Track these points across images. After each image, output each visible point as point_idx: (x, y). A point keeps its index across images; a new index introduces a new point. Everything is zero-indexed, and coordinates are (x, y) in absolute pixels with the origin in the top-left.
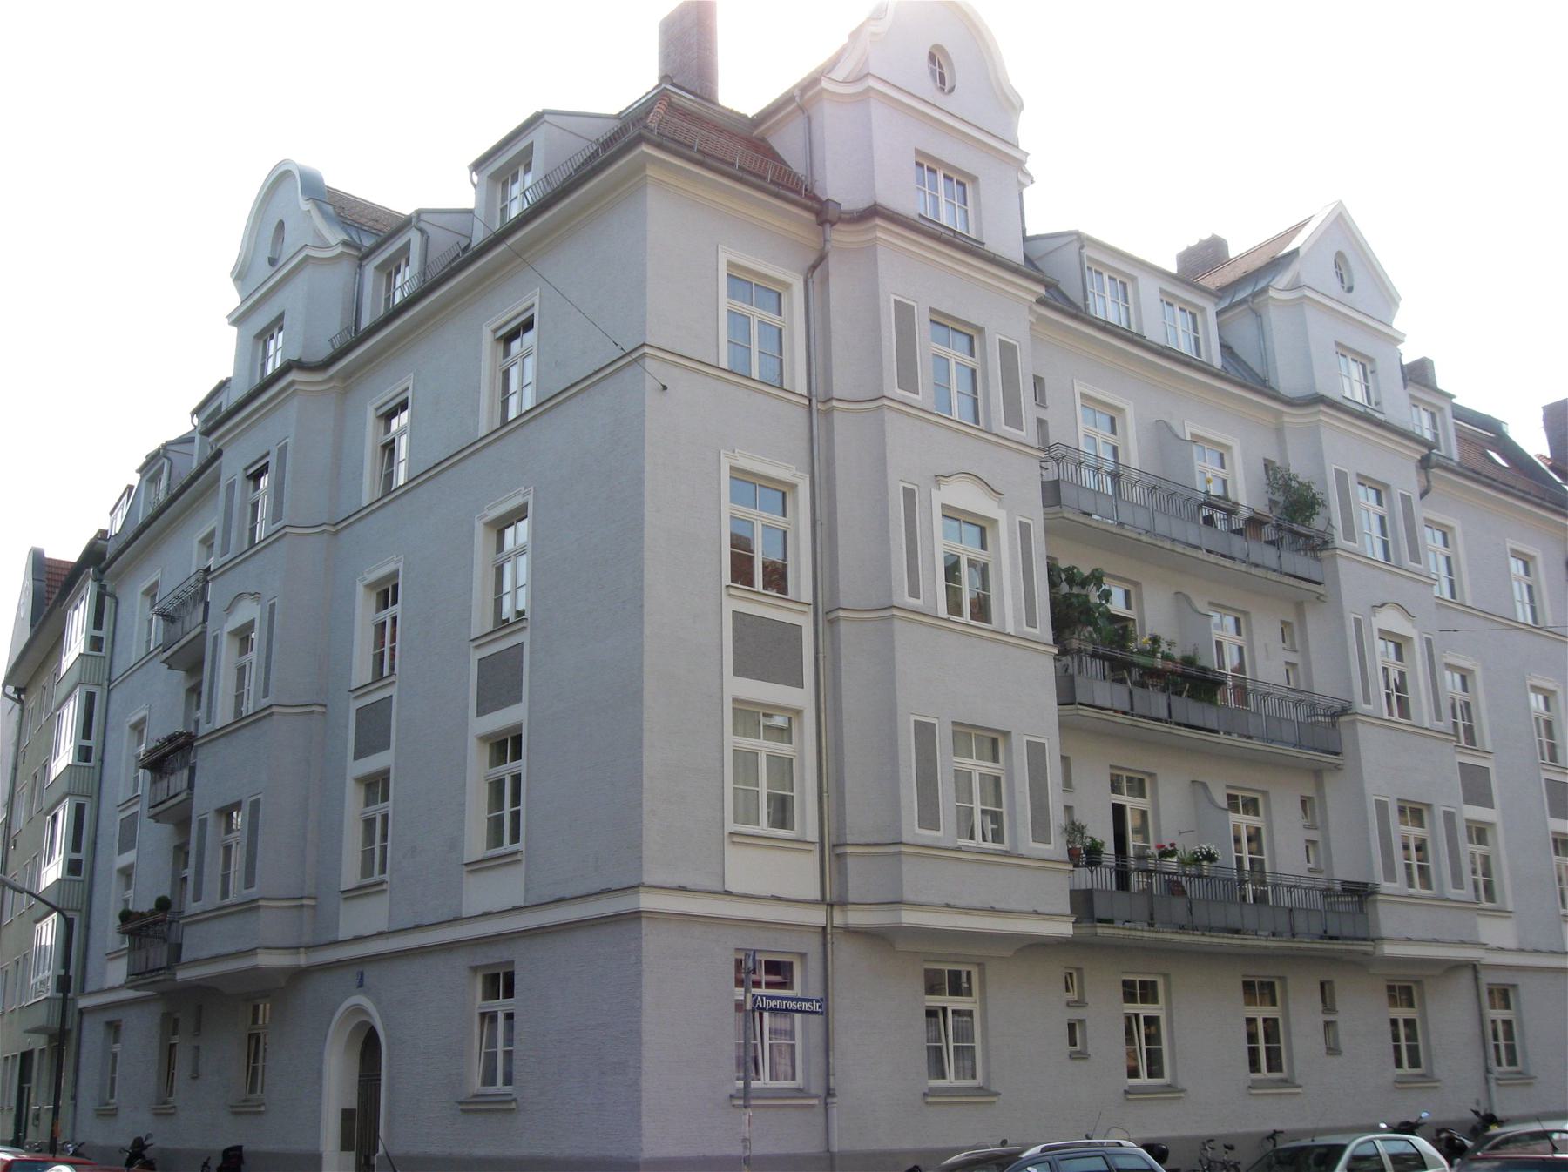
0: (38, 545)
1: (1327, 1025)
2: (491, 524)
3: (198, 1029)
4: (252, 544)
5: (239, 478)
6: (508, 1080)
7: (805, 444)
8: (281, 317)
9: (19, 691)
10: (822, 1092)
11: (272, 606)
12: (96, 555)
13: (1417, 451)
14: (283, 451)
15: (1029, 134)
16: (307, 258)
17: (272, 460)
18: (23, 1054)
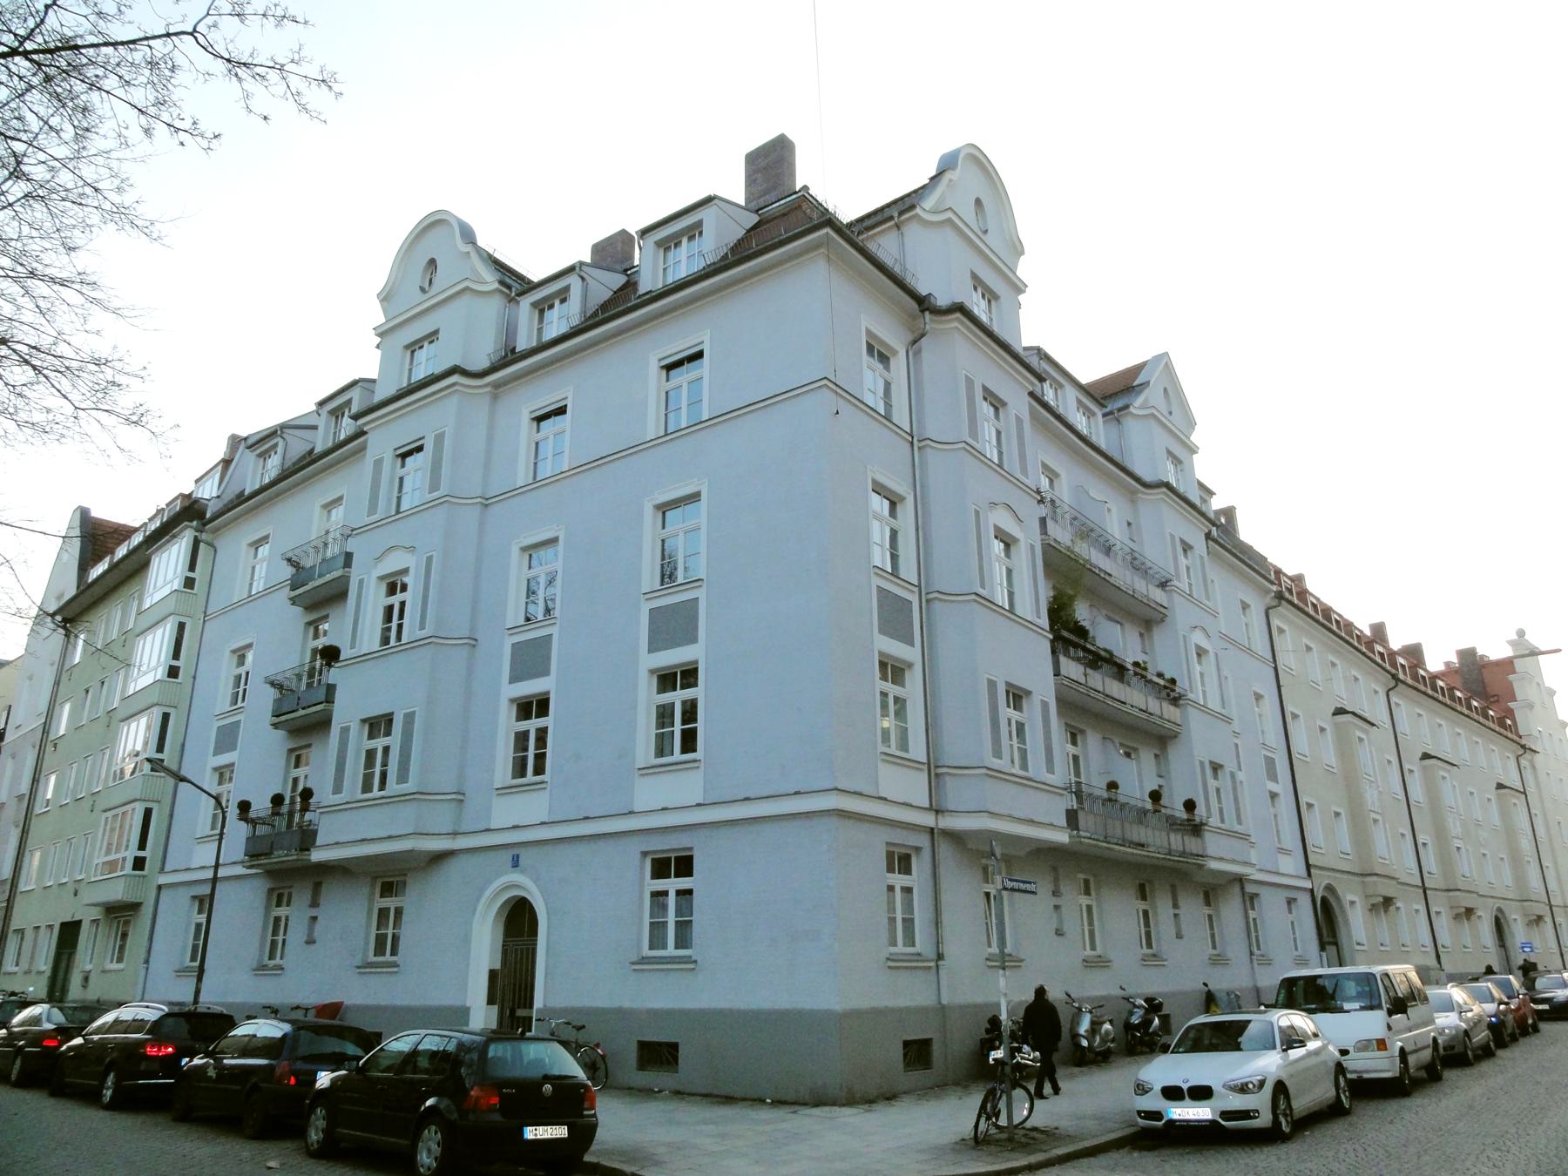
0: (85, 505)
1: (1176, 915)
2: (658, 507)
3: (315, 904)
4: (398, 512)
5: (388, 456)
6: (394, 953)
7: (910, 470)
8: (436, 332)
9: (65, 620)
10: (934, 956)
11: (429, 559)
12: (189, 512)
13: (883, 561)
14: (439, 439)
15: (1025, 269)
16: (467, 289)
17: (429, 445)
18: (63, 925)
